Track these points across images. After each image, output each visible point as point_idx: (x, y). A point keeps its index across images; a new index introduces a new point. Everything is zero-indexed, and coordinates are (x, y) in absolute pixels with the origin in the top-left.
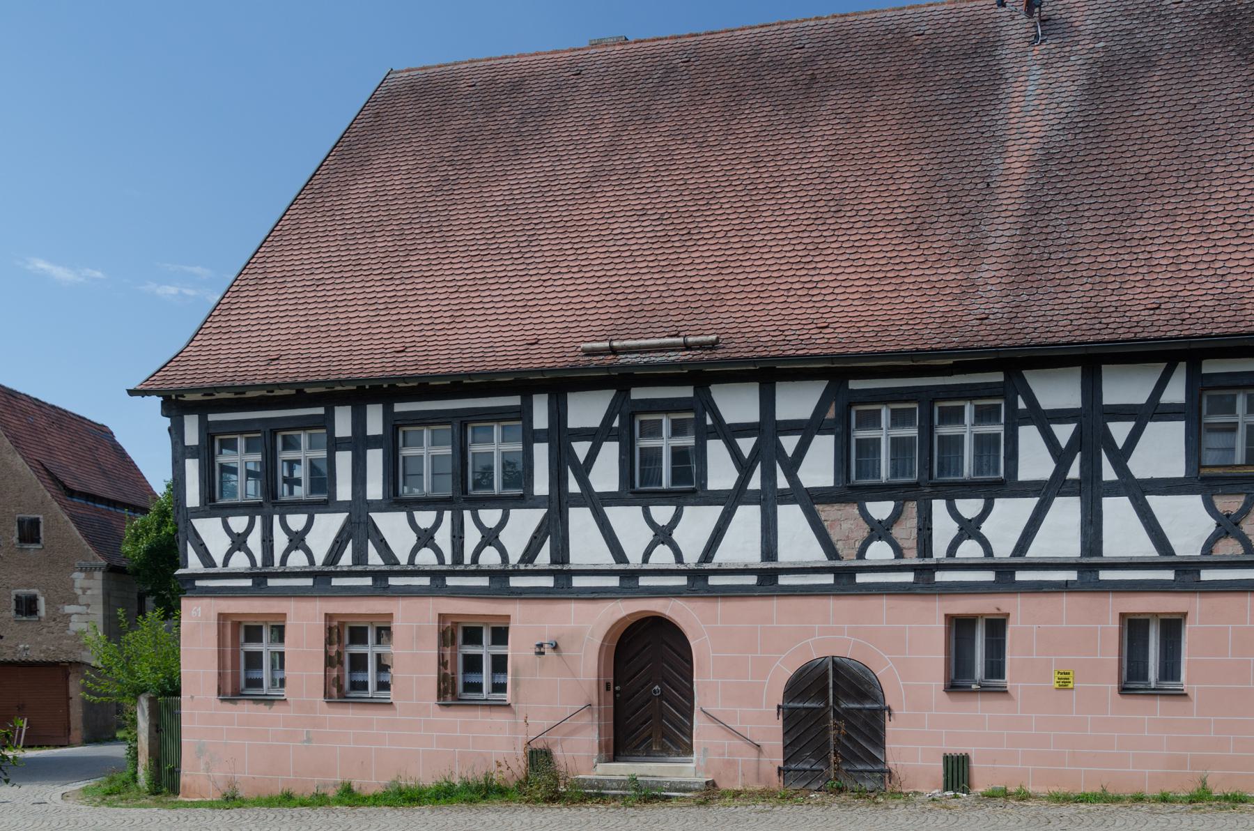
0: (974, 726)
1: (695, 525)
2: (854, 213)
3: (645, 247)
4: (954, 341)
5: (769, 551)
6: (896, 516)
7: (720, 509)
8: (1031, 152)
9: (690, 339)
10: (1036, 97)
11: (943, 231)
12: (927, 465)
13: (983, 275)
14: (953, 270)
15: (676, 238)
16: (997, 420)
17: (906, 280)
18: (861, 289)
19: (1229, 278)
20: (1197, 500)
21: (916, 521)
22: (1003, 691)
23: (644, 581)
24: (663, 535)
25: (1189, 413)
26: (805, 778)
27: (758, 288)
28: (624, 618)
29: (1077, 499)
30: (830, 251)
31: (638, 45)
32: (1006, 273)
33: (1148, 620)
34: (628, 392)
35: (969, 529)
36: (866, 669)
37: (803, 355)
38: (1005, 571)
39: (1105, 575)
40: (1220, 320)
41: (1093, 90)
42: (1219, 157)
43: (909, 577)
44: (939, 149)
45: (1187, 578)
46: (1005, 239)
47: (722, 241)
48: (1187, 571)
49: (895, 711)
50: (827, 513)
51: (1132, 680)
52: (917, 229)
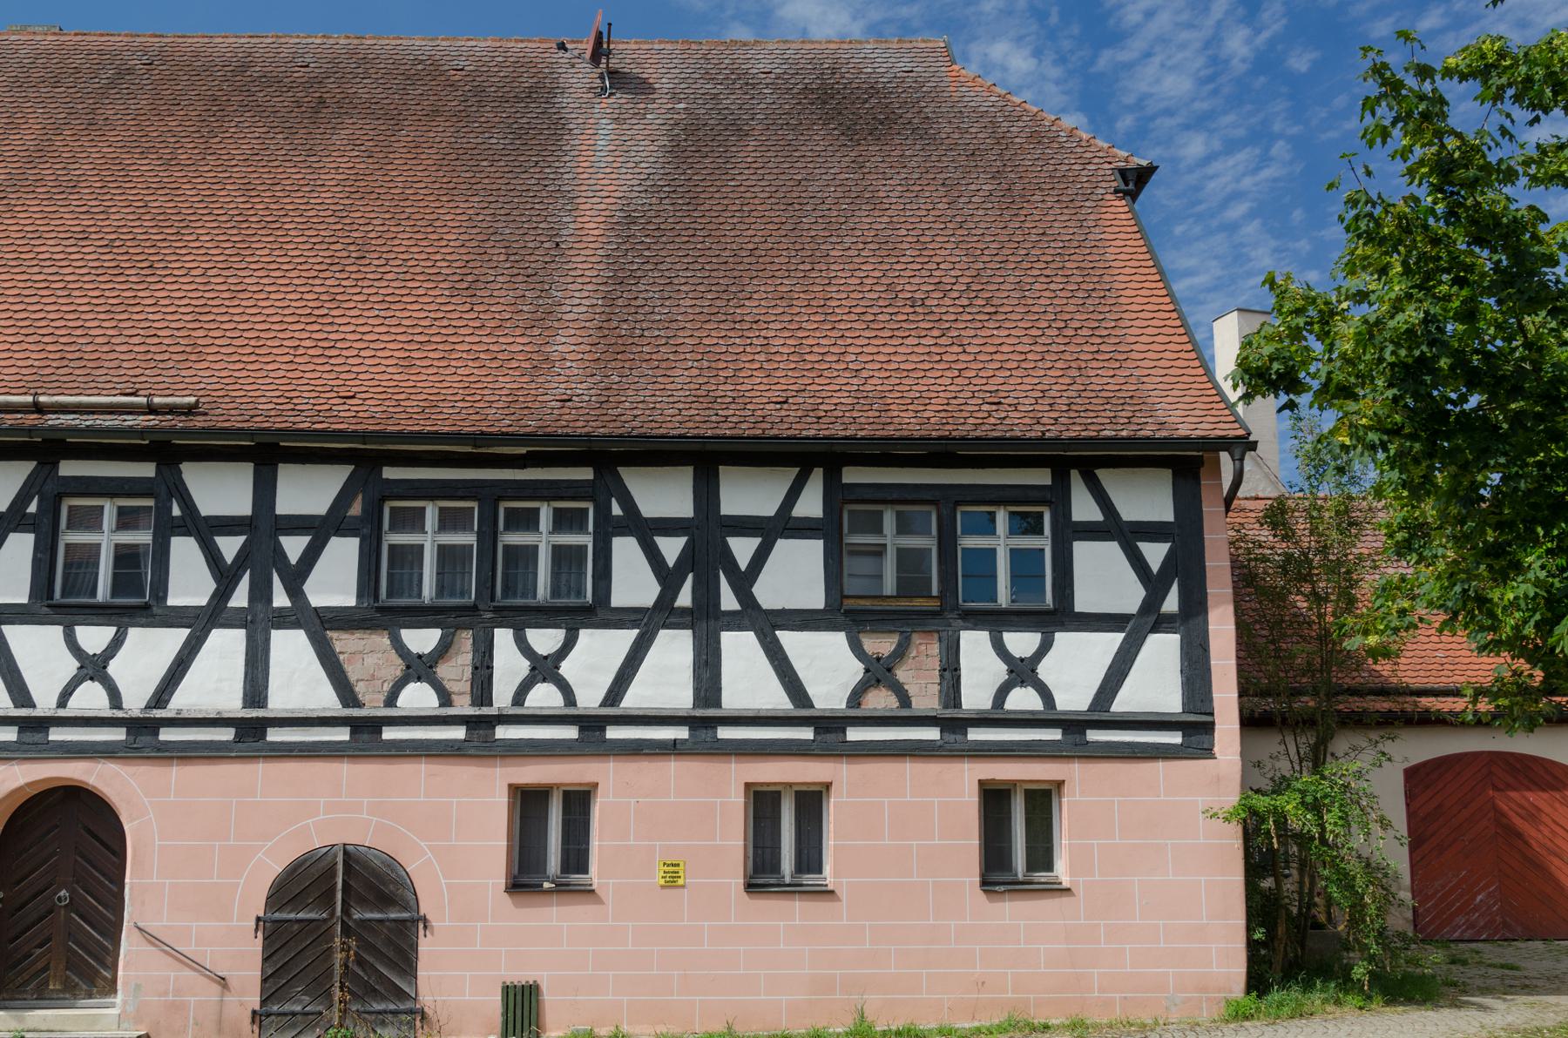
0: (545, 942)
1: (143, 656)
2: (382, 262)
3: (86, 278)
4: (531, 425)
5: (255, 691)
6: (443, 650)
7: (184, 633)
8: (607, 213)
9: (157, 400)
10: (608, 156)
11: (503, 293)
12: (487, 583)
13: (559, 348)
14: (519, 340)
15: (133, 272)
16: (582, 529)
17: (457, 347)
18: (397, 354)
19: (865, 374)
20: (840, 638)
21: (470, 656)
22: (588, 892)
23: (56, 735)
24: (94, 668)
25: (825, 529)
26: (293, 1026)
27: (253, 343)
28: (20, 789)
29: (689, 632)
30: (352, 305)
31: (79, 38)
32: (588, 348)
33: (779, 793)
34: (55, 465)
35: (545, 669)
36: (392, 862)
37: (323, 430)
38: (591, 725)
39: (724, 733)
40: (863, 420)
41: (675, 151)
42: (834, 239)
43: (459, 733)
44: (491, 199)
45: (831, 737)
46: (584, 309)
47: (198, 280)
48: (829, 725)
49: (435, 922)
50: (343, 642)
51: (762, 875)
52: (470, 287)
